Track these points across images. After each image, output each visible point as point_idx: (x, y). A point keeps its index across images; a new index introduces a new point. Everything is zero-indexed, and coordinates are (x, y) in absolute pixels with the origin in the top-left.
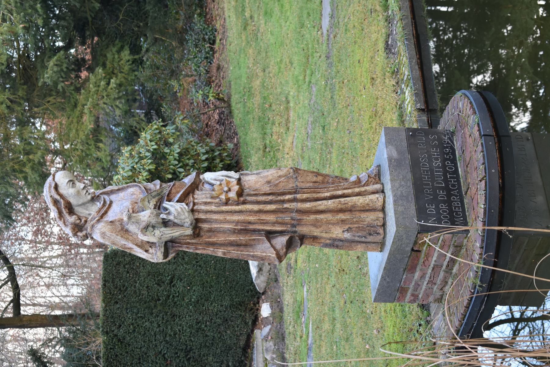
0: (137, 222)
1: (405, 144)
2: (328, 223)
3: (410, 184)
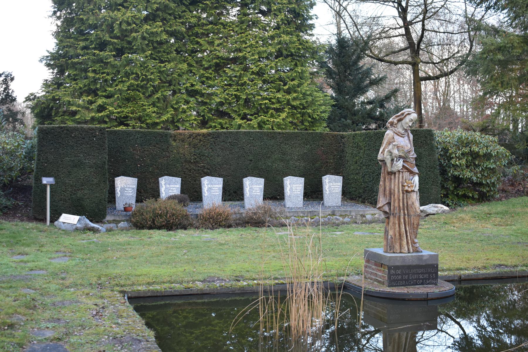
0: (393, 149)
1: (430, 263)
2: (395, 229)
3: (410, 264)
